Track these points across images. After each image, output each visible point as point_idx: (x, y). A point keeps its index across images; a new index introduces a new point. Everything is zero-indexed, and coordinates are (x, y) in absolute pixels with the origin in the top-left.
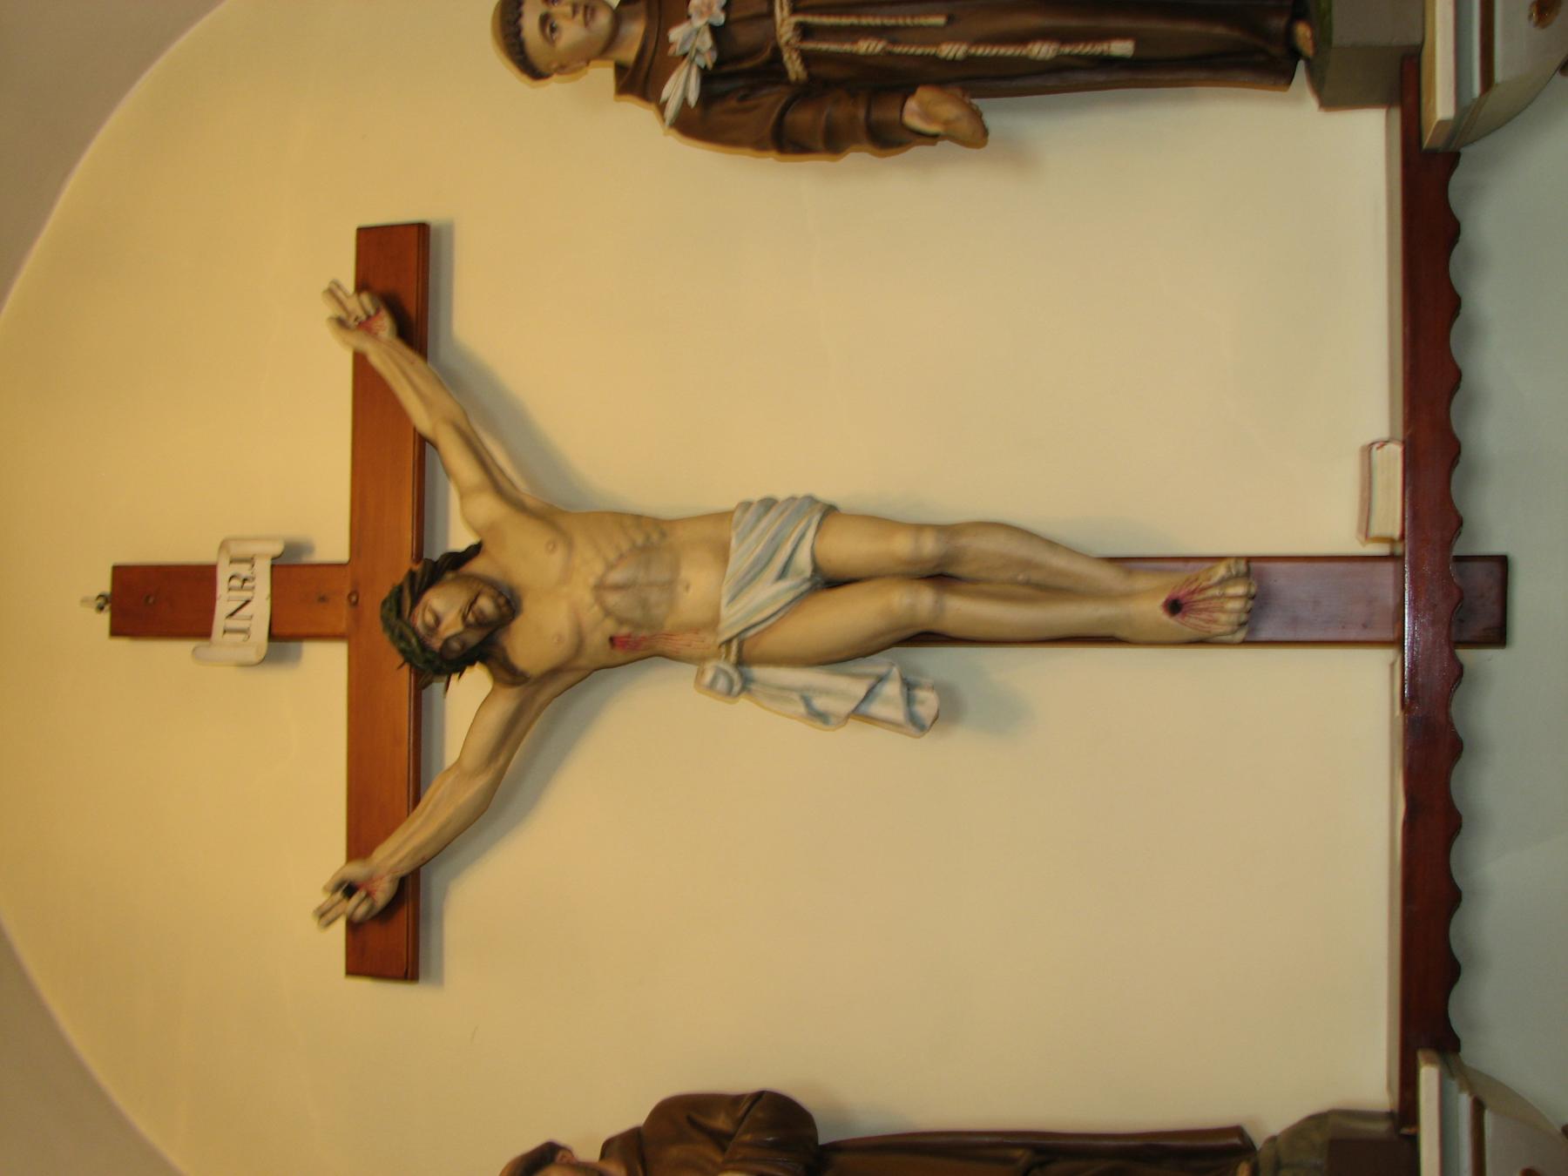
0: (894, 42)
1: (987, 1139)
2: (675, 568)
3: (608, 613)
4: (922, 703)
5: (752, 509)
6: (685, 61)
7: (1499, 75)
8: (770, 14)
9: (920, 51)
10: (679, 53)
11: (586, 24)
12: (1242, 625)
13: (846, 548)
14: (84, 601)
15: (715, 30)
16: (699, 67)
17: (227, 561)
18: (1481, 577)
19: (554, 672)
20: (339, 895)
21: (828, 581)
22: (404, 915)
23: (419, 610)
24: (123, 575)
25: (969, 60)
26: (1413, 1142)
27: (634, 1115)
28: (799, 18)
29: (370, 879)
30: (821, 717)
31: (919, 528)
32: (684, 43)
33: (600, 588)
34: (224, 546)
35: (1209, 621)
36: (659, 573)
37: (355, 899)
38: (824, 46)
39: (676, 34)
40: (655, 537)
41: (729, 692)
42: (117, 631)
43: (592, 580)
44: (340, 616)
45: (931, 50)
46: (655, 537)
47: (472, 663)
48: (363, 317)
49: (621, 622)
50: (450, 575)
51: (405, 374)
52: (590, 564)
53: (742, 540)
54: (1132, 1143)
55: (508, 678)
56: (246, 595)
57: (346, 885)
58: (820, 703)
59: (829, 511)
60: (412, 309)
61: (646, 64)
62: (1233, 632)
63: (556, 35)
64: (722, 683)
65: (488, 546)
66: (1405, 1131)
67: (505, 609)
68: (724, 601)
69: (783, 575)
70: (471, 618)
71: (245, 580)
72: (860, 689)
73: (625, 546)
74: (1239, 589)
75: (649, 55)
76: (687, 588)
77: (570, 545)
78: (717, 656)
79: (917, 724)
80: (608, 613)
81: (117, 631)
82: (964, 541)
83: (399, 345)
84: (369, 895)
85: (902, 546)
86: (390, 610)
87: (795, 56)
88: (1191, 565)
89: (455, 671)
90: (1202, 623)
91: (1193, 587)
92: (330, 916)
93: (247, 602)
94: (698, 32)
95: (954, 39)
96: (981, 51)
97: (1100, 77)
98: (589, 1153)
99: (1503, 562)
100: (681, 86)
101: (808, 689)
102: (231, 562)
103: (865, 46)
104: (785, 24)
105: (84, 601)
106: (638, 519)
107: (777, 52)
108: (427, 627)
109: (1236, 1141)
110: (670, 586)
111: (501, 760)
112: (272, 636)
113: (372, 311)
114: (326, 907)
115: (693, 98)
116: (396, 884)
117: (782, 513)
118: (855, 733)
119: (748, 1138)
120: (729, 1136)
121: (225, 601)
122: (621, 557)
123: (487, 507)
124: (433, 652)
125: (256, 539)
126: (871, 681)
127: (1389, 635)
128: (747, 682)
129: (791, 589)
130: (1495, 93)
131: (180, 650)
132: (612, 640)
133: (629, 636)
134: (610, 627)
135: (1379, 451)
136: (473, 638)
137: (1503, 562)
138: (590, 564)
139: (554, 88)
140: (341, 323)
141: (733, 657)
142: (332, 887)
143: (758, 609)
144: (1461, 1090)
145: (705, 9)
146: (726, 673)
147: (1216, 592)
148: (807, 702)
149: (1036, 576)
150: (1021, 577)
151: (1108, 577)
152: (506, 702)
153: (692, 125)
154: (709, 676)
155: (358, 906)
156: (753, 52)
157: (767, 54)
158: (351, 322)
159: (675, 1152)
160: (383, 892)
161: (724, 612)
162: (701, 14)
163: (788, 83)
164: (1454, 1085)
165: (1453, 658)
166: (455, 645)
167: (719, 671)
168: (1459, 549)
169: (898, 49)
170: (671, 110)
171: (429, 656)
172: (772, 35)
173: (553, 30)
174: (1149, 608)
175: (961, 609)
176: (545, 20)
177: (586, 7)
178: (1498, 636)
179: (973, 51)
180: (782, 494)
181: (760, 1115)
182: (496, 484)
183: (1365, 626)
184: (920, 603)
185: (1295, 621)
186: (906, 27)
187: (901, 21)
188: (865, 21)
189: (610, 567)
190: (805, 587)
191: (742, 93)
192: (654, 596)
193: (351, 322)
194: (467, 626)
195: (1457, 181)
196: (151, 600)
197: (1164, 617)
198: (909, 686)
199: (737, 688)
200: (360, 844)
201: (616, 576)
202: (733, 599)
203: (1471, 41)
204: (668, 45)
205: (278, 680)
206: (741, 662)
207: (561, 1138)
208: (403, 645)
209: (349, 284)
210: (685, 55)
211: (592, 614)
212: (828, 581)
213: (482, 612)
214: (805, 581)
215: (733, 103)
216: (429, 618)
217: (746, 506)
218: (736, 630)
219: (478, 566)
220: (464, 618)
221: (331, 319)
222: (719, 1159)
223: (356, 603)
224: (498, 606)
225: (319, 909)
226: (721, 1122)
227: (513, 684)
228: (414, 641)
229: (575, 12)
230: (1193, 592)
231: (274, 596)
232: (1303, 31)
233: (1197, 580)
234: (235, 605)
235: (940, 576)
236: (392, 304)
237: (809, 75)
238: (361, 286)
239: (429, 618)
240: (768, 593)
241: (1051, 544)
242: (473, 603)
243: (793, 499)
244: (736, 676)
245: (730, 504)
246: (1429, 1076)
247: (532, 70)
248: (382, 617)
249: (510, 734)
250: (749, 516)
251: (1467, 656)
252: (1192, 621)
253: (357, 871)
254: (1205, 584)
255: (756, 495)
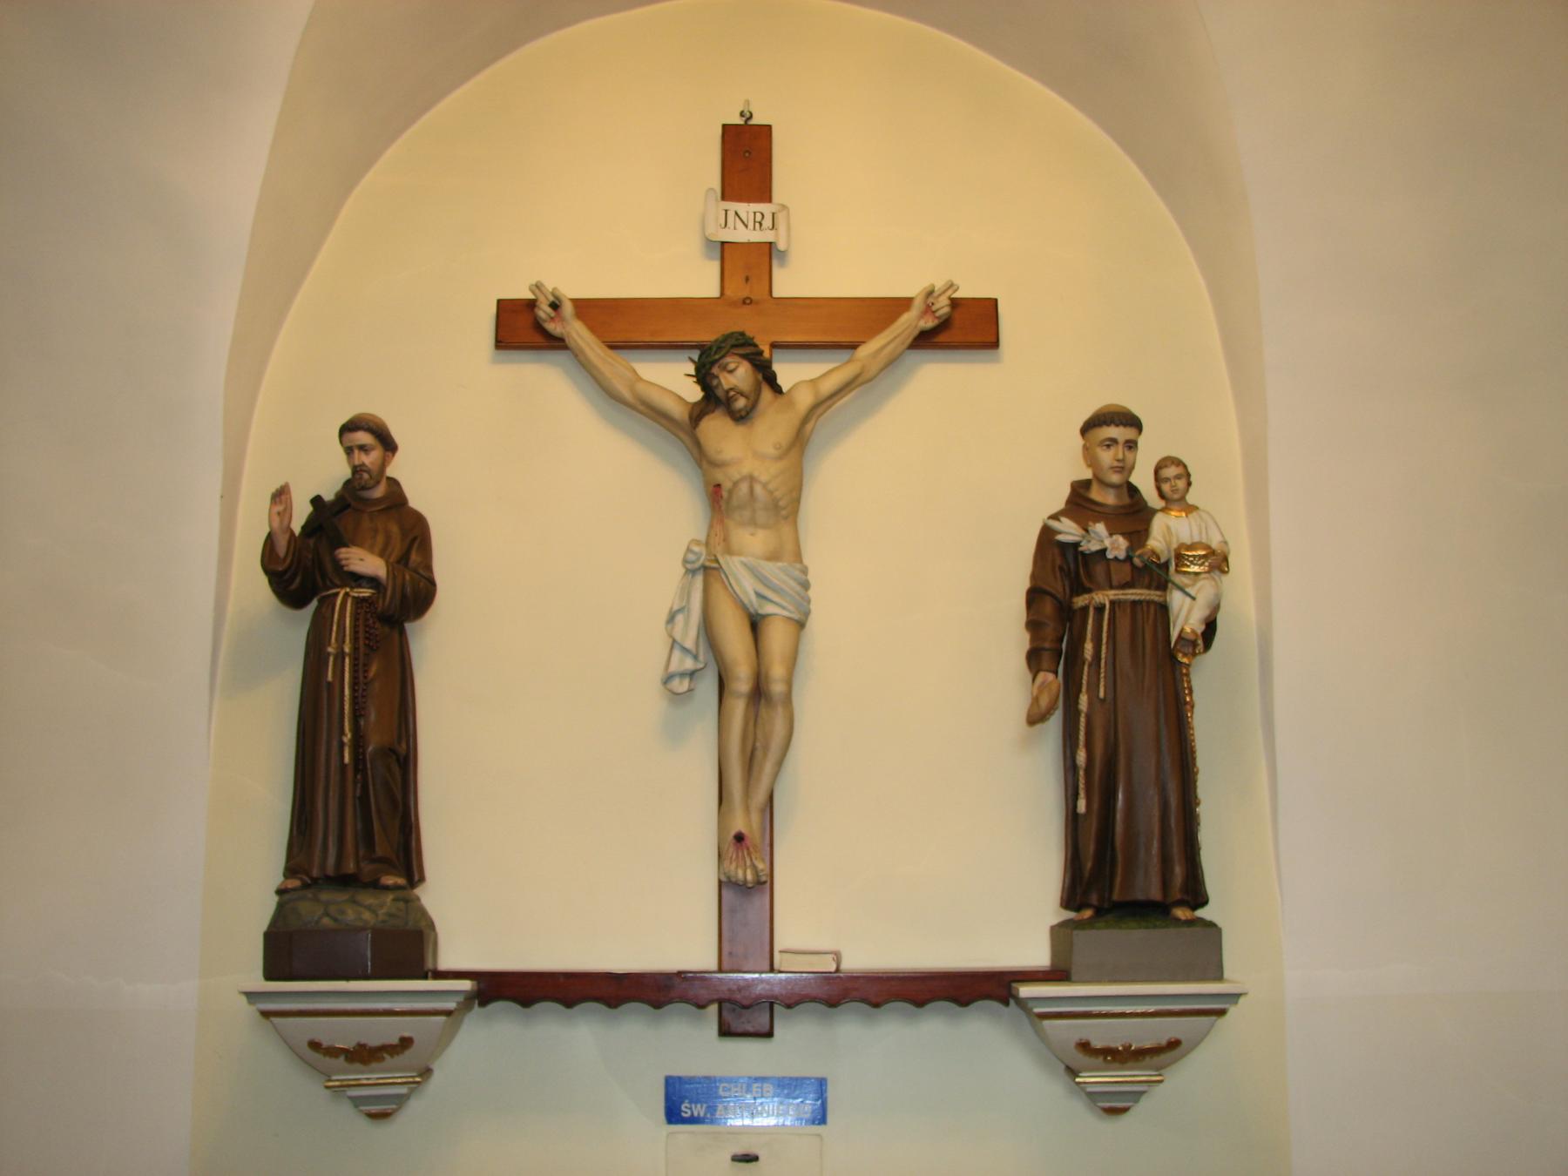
0: (1090, 665)
1: (411, 726)
2: (765, 527)
3: (736, 484)
4: (681, 682)
5: (804, 577)
6: (1084, 532)
7: (1046, 1023)
8: (1111, 587)
9: (1084, 682)
10: (1090, 528)
11: (1112, 468)
12: (729, 878)
13: (777, 637)
14: (747, 102)
15: (1103, 551)
16: (1081, 542)
17: (774, 211)
18: (761, 1021)
19: (697, 444)
20: (551, 298)
21: (756, 624)
22: (539, 339)
23: (737, 359)
24: (764, 133)
25: (1078, 713)
26: (425, 977)
27: (416, 501)
28: (1108, 606)
29: (562, 319)
30: (671, 619)
31: (789, 683)
32: (1095, 533)
33: (751, 479)
34: (784, 207)
35: (731, 858)
36: (762, 516)
37: (549, 310)
38: (1090, 621)
39: (1100, 528)
40: (784, 513)
41: (685, 561)
42: (727, 129)
43: (756, 474)
44: (737, 290)
45: (1084, 689)
46: (784, 513)
47: (704, 389)
48: (934, 308)
49: (730, 492)
50: (760, 377)
51: (895, 338)
52: (768, 473)
53: (780, 568)
54: (413, 818)
55: (696, 413)
56: (751, 225)
57: (557, 302)
58: (680, 618)
59: (801, 625)
60: (941, 338)
61: (1088, 505)
62: (725, 873)
63: (1105, 448)
64: (691, 557)
65: (781, 400)
66: (430, 974)
67: (738, 415)
68: (743, 559)
69: (758, 595)
70: (732, 393)
71: (761, 224)
72: (689, 643)
73: (778, 494)
74: (749, 877)
75: (1093, 507)
76: (752, 535)
77: (780, 458)
78: (709, 553)
79: (668, 679)
80: (736, 484)
81: (727, 129)
82: (780, 710)
83: (916, 333)
84: (552, 319)
85: (777, 671)
86: (737, 340)
87: (1087, 602)
88: (768, 849)
89: (698, 380)
90: (730, 855)
91: (751, 849)
92: (537, 291)
93: (746, 226)
94: (1102, 541)
95: (1090, 704)
96: (1083, 720)
97: (1070, 792)
98: (391, 471)
99: (769, 1034)
100: (1069, 530)
101: (689, 611)
102: (773, 214)
103: (1089, 647)
104: (1104, 597)
105: (747, 102)
106: (797, 501)
107: (1089, 591)
108: (727, 364)
109: (416, 878)
110: (753, 523)
111: (641, 408)
112: (723, 243)
113: (938, 314)
114: (543, 289)
115: (1060, 538)
116: (559, 336)
117: (799, 595)
118: (660, 646)
119: (407, 577)
120: (406, 565)
121: (746, 209)
122: (771, 493)
123: (804, 400)
124: (711, 368)
125: (789, 229)
126: (694, 651)
127: (725, 966)
128: (693, 572)
129: (750, 602)
130: (1037, 1020)
131: (716, 183)
132: (718, 486)
133: (722, 497)
134: (727, 485)
135: (831, 959)
136: (720, 393)
137: (769, 1034)
138: (768, 473)
139: (1079, 441)
140: (930, 293)
141: (708, 564)
142: (557, 293)
143: (737, 580)
144: (458, 1003)
145: (1116, 546)
146: (698, 559)
147: (748, 863)
148: (680, 610)
149: (759, 753)
150: (758, 744)
151: (760, 797)
152: (679, 412)
153: (1047, 535)
154: (696, 549)
155: (545, 312)
156: (1089, 575)
157: (1087, 584)
158: (931, 300)
159: (395, 529)
160: (554, 328)
161: (736, 559)
162: (1112, 543)
163: (1071, 596)
164: (461, 998)
165: (711, 1002)
166: (715, 382)
167: (698, 555)
168: (777, 1008)
169: (1086, 668)
170: (1054, 524)
171: (708, 367)
172: (1100, 588)
173: (1108, 446)
174: (738, 824)
175: (738, 708)
176: (1114, 441)
177: (1122, 468)
178: (725, 1032)
179: (1083, 715)
180: (811, 593)
181: (422, 584)
182: (821, 405)
183: (730, 954)
184: (742, 683)
185: (733, 911)
186: (1099, 674)
187: (1102, 670)
188: (1104, 648)
189: (765, 486)
190: (752, 610)
191: (1065, 567)
192: (747, 514)
193: (931, 300)
194: (727, 392)
195: (995, 1005)
196: (747, 154)
197: (733, 833)
198: (692, 674)
199: (689, 566)
200: (584, 308)
201: (758, 489)
202: (745, 565)
203: (1044, 1007)
204: (1096, 520)
205: (694, 245)
206: (705, 568)
207: (399, 454)
208: (714, 349)
209: (956, 295)
210: (1087, 531)
211: (735, 473)
212: (756, 624)
213: (736, 400)
214: (756, 611)
215: (1058, 562)
216: (732, 366)
217: (805, 571)
218: (724, 566)
219: (767, 394)
220: (731, 389)
221: (933, 286)
222: (391, 560)
223: (744, 303)
224: (740, 411)
225: (542, 285)
226: (415, 557)
227: (691, 417)
228: (717, 357)
229: (1118, 460)
230: (748, 849)
231: (750, 244)
232: (1088, 913)
233: (756, 852)
234: (743, 216)
235: (759, 693)
236: (944, 325)
237: (1076, 610)
238: (955, 303)
239: (732, 366)
240: (747, 586)
241: (780, 763)
242: (742, 394)
243: (809, 601)
244: (697, 565)
245: (806, 561)
246: (466, 985)
247: (1087, 428)
248: (733, 333)
249: (656, 414)
250: (797, 574)
251: (713, 1009)
252: (731, 850)
253: (568, 309)
254: (753, 857)
255: (811, 578)
